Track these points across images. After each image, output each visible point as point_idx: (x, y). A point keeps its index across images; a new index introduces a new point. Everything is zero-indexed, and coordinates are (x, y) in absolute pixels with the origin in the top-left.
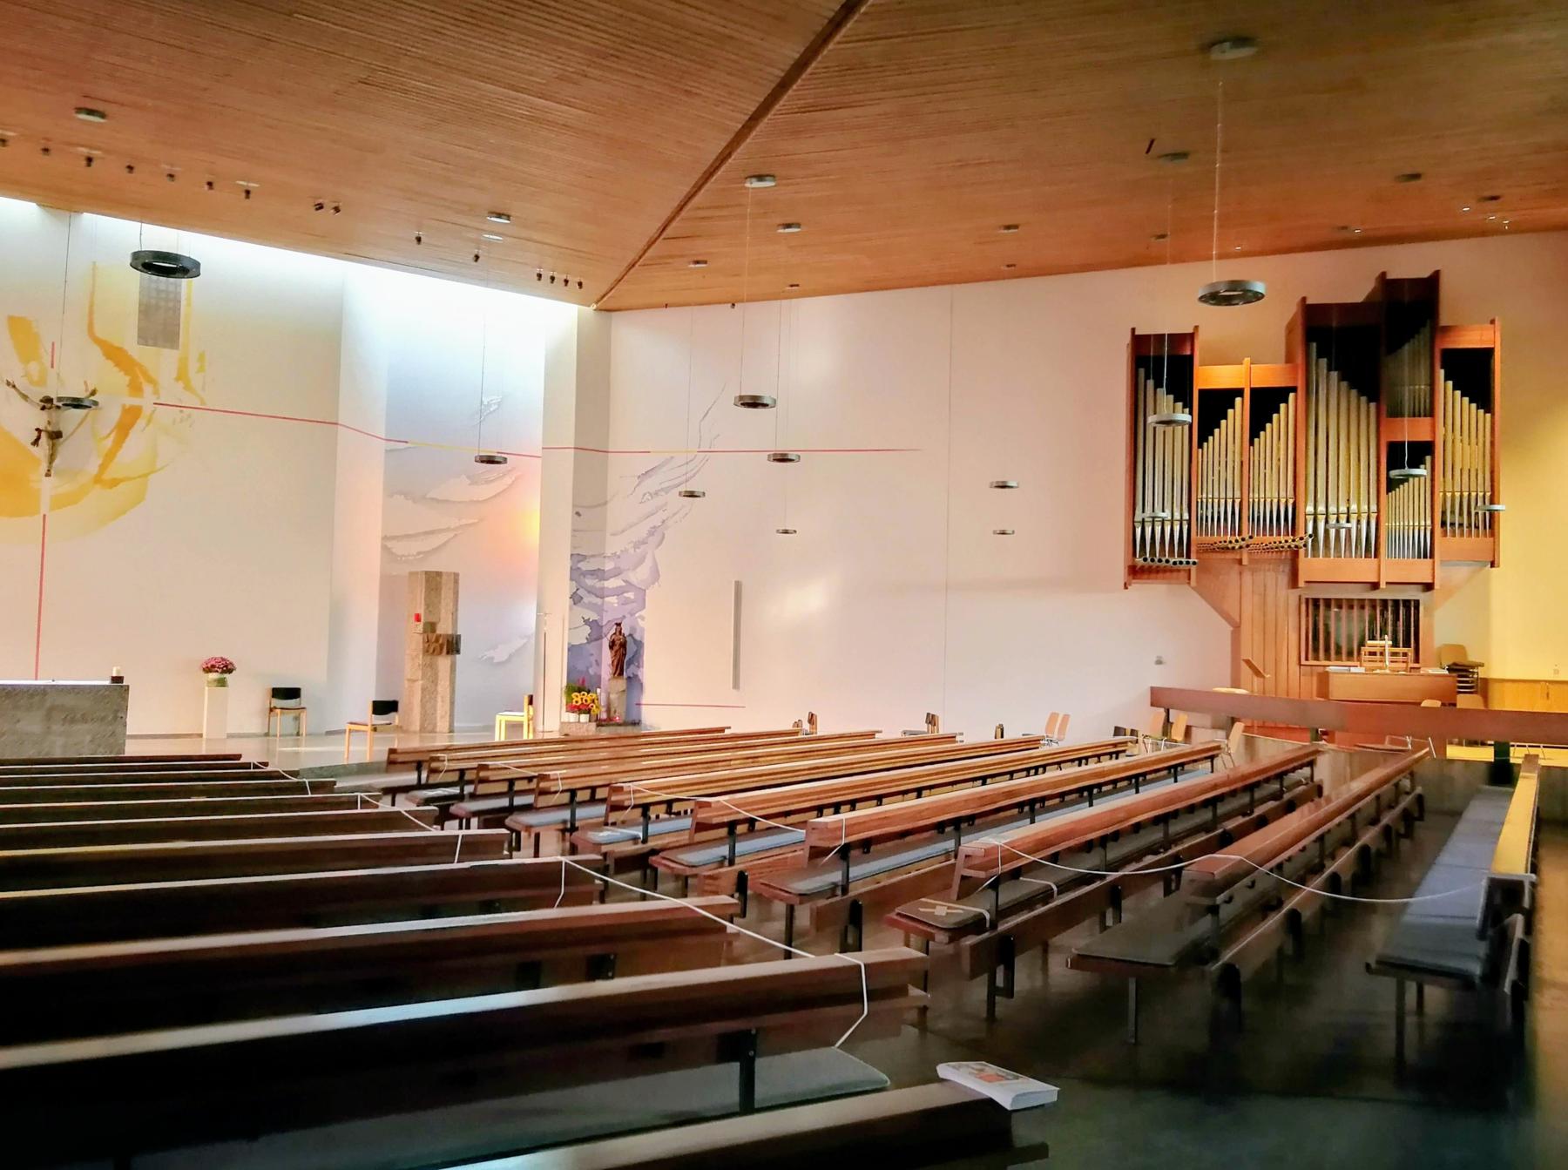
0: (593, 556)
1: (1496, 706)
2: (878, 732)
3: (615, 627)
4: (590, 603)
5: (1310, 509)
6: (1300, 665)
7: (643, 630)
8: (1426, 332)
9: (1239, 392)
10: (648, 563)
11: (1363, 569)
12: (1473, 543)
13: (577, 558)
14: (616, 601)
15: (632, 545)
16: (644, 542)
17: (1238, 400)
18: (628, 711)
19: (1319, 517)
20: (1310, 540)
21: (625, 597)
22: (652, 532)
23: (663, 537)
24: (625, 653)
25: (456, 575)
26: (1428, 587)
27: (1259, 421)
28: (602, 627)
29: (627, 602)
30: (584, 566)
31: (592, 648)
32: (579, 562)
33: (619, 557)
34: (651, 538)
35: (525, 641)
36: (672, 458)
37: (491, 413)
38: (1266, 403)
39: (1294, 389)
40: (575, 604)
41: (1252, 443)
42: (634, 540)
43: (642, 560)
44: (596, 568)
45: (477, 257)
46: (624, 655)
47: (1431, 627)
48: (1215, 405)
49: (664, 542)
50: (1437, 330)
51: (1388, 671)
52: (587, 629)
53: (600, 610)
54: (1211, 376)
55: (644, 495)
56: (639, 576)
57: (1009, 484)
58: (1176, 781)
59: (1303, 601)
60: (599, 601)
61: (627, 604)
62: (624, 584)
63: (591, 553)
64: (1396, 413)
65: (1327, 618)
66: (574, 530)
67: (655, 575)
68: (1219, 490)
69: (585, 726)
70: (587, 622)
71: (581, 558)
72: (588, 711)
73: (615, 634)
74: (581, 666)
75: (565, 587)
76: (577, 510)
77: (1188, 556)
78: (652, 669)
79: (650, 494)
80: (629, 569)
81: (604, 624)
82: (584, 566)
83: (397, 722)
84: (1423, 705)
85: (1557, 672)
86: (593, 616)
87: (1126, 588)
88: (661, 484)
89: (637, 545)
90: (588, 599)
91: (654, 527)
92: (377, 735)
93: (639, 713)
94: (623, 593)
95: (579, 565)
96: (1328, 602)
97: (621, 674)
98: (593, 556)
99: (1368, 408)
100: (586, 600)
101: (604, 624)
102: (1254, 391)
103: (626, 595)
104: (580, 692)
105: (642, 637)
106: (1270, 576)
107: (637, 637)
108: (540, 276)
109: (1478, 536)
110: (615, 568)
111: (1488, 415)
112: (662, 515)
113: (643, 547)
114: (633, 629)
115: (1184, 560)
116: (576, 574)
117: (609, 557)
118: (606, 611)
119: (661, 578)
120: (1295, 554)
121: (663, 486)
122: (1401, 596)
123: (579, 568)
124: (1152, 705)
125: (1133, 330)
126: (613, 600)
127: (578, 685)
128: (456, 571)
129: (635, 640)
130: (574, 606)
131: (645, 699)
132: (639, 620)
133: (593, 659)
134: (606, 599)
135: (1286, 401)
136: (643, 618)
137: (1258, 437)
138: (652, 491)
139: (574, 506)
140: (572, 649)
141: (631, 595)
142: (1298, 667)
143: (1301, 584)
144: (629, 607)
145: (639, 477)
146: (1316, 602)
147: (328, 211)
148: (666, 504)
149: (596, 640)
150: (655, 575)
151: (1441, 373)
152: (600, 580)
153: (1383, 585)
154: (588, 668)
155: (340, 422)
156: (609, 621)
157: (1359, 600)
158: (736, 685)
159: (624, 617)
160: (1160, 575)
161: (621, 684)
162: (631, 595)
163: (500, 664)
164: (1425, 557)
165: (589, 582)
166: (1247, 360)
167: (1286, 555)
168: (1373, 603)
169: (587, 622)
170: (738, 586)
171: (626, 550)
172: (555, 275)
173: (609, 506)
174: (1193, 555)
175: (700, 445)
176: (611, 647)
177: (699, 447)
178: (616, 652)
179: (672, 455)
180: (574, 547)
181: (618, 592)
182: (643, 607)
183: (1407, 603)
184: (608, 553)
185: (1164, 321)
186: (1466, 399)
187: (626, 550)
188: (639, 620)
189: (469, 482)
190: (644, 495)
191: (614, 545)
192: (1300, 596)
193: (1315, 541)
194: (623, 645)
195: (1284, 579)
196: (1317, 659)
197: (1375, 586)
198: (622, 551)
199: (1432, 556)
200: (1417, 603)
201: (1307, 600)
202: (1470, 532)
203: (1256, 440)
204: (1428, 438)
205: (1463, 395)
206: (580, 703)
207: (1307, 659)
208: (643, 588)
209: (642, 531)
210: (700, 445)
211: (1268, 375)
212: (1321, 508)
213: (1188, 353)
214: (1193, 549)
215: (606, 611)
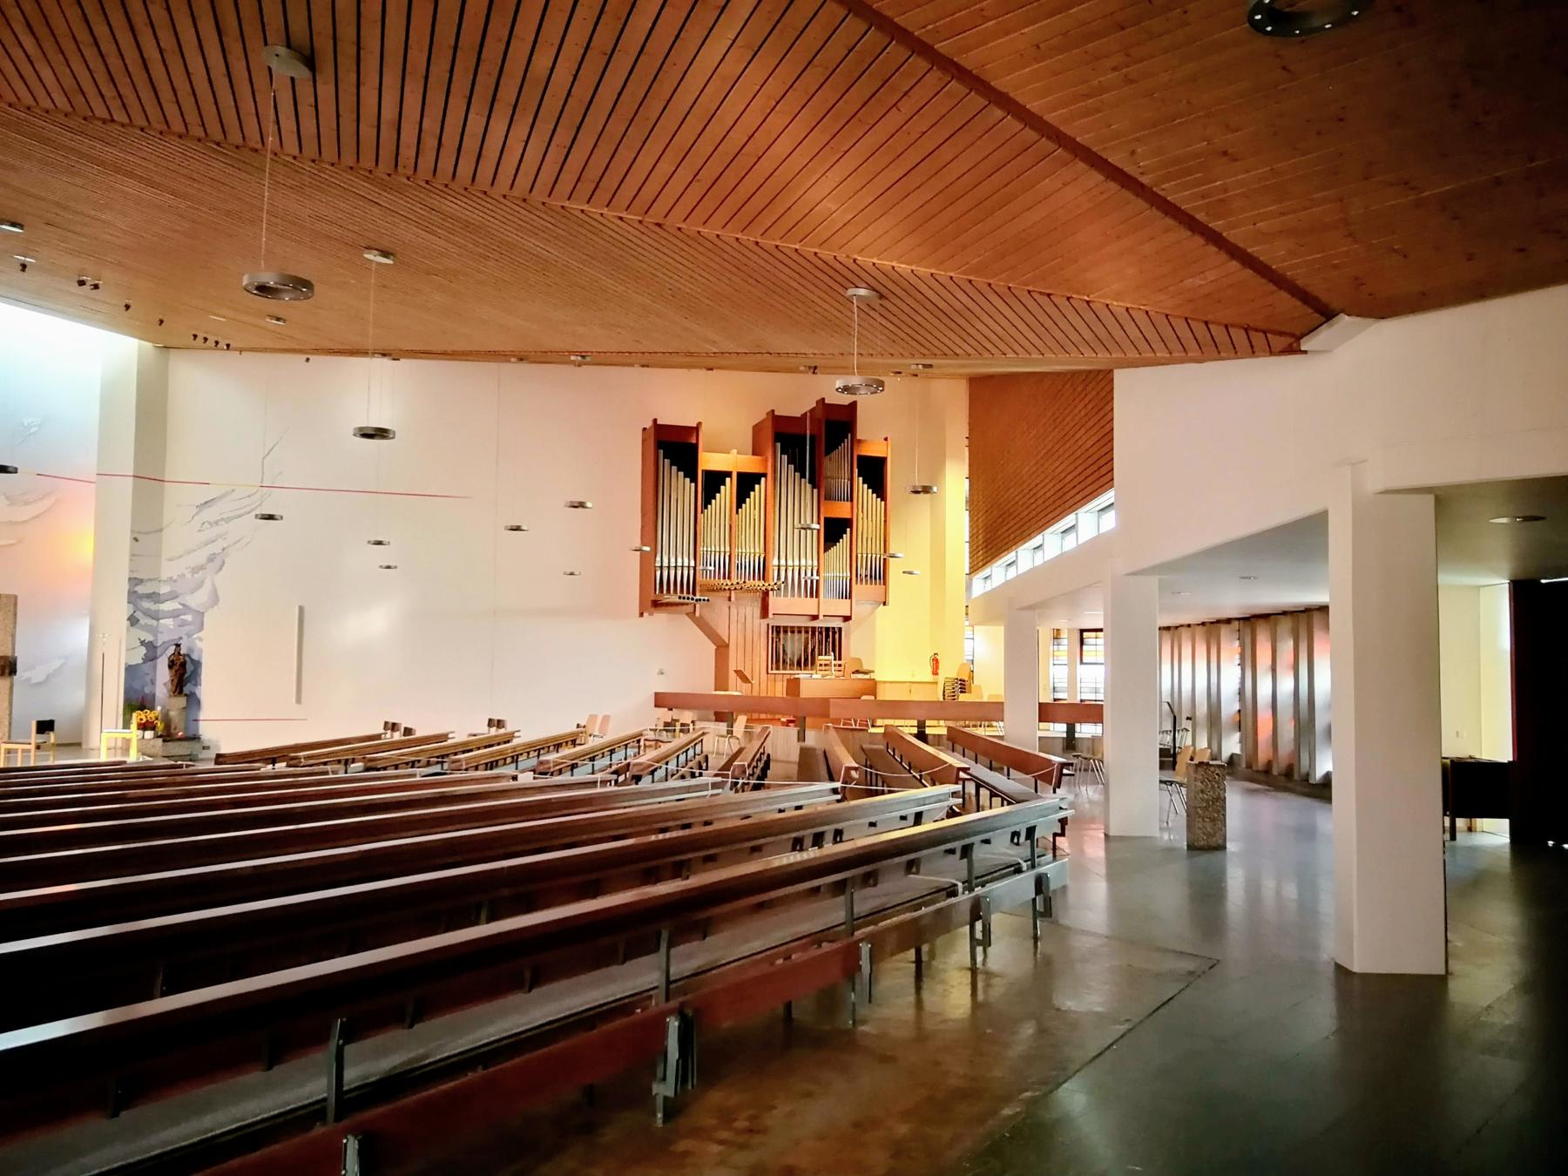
0: (150, 580)
1: (880, 697)
2: (451, 732)
3: (174, 647)
4: (146, 624)
5: (775, 562)
6: (768, 673)
7: (201, 651)
8: (848, 442)
9: (729, 474)
10: (207, 588)
11: (807, 606)
12: (872, 589)
13: (134, 581)
14: (172, 623)
15: (190, 570)
16: (202, 568)
17: (728, 480)
18: (186, 729)
19: (781, 568)
20: (783, 585)
21: (182, 619)
22: (211, 559)
23: (223, 563)
24: (184, 672)
25: (16, 597)
26: (847, 619)
27: (742, 496)
28: (156, 647)
29: (183, 624)
30: (141, 589)
31: (147, 667)
32: (136, 585)
33: (175, 581)
34: (210, 565)
35: (63, 661)
36: (233, 490)
37: (30, 435)
38: (747, 483)
39: (765, 475)
40: (132, 625)
41: (737, 513)
42: (192, 566)
43: (200, 585)
44: (151, 592)
45: (161, 322)
46: (184, 674)
47: (848, 649)
48: (714, 481)
49: (224, 568)
50: (856, 442)
51: (833, 677)
52: (143, 650)
53: (154, 631)
54: (709, 461)
55: (203, 524)
56: (196, 600)
57: (523, 528)
58: (572, 775)
59: (770, 627)
60: (154, 623)
61: (183, 626)
62: (181, 607)
63: (148, 577)
64: (828, 498)
65: (785, 639)
66: (133, 555)
67: (215, 599)
68: (714, 544)
69: (152, 742)
70: (143, 643)
71: (136, 582)
72: (153, 728)
73: (174, 654)
74: (137, 685)
75: (124, 610)
76: (136, 535)
77: (694, 594)
78: (209, 687)
79: (210, 523)
80: (186, 593)
81: (159, 645)
82: (141, 589)
83: (52, 741)
84: (862, 698)
85: (913, 676)
86: (149, 638)
87: (641, 615)
88: (221, 514)
89: (195, 570)
90: (144, 621)
91: (214, 554)
92: (39, 753)
93: (197, 729)
94: (178, 616)
95: (137, 589)
96: (785, 630)
97: (181, 692)
98: (150, 580)
99: (813, 491)
100: (142, 622)
101: (159, 645)
102: (739, 474)
103: (182, 617)
104: (142, 710)
105: (200, 657)
106: (749, 610)
107: (195, 657)
108: (195, 336)
109: (876, 584)
110: (170, 592)
111: (883, 503)
112: (221, 544)
113: (201, 572)
114: (191, 650)
115: (691, 596)
116: (133, 597)
117: (165, 581)
118: (162, 633)
119: (221, 602)
120: (766, 594)
121: (225, 516)
122: (830, 625)
123: (136, 592)
124: (656, 706)
125: (655, 420)
126: (168, 622)
127: (136, 702)
128: (16, 594)
129: (192, 660)
130: (131, 629)
131: (202, 715)
132: (197, 641)
133: (148, 678)
134: (161, 621)
135: (759, 483)
136: (201, 639)
137: (710, 504)
138: (212, 520)
139: (132, 531)
140: (130, 670)
141: (188, 618)
142: (766, 675)
143: (770, 616)
144: (187, 628)
145: (197, 507)
146: (778, 628)
147: (86, 288)
148: (227, 533)
149: (152, 660)
150: (215, 599)
151: (856, 471)
152: (155, 603)
153: (821, 617)
154: (143, 687)
155: (132, 478)
156: (164, 643)
157: (805, 627)
158: (299, 700)
159: (181, 638)
160: (663, 608)
161: (182, 701)
162: (188, 618)
163: (38, 684)
164: (846, 598)
165: (146, 604)
166: (735, 451)
167: (759, 595)
168: (814, 629)
169: (143, 643)
170: (301, 610)
171: (183, 575)
172: (220, 339)
173: (164, 533)
174: (698, 594)
175: (262, 480)
176: (170, 667)
177: (262, 482)
178: (176, 671)
179: (234, 487)
180: (132, 571)
181: (174, 615)
182: (201, 628)
183: (827, 629)
184: (164, 577)
185: (676, 415)
186: (870, 491)
187: (183, 575)
188: (197, 641)
189: (8, 502)
190: (203, 524)
191: (168, 570)
192: (768, 625)
193: (786, 587)
194: (183, 665)
195: (757, 611)
196: (778, 669)
197: (815, 618)
198: (179, 576)
199: (850, 598)
200: (840, 629)
201: (773, 627)
202: (866, 581)
203: (740, 510)
204: (848, 516)
205: (868, 488)
206: (145, 720)
207: (772, 669)
208: (201, 611)
209: (200, 557)
210: (262, 480)
211: (749, 464)
212: (783, 562)
213: (694, 442)
214: (698, 588)
215: (162, 633)
